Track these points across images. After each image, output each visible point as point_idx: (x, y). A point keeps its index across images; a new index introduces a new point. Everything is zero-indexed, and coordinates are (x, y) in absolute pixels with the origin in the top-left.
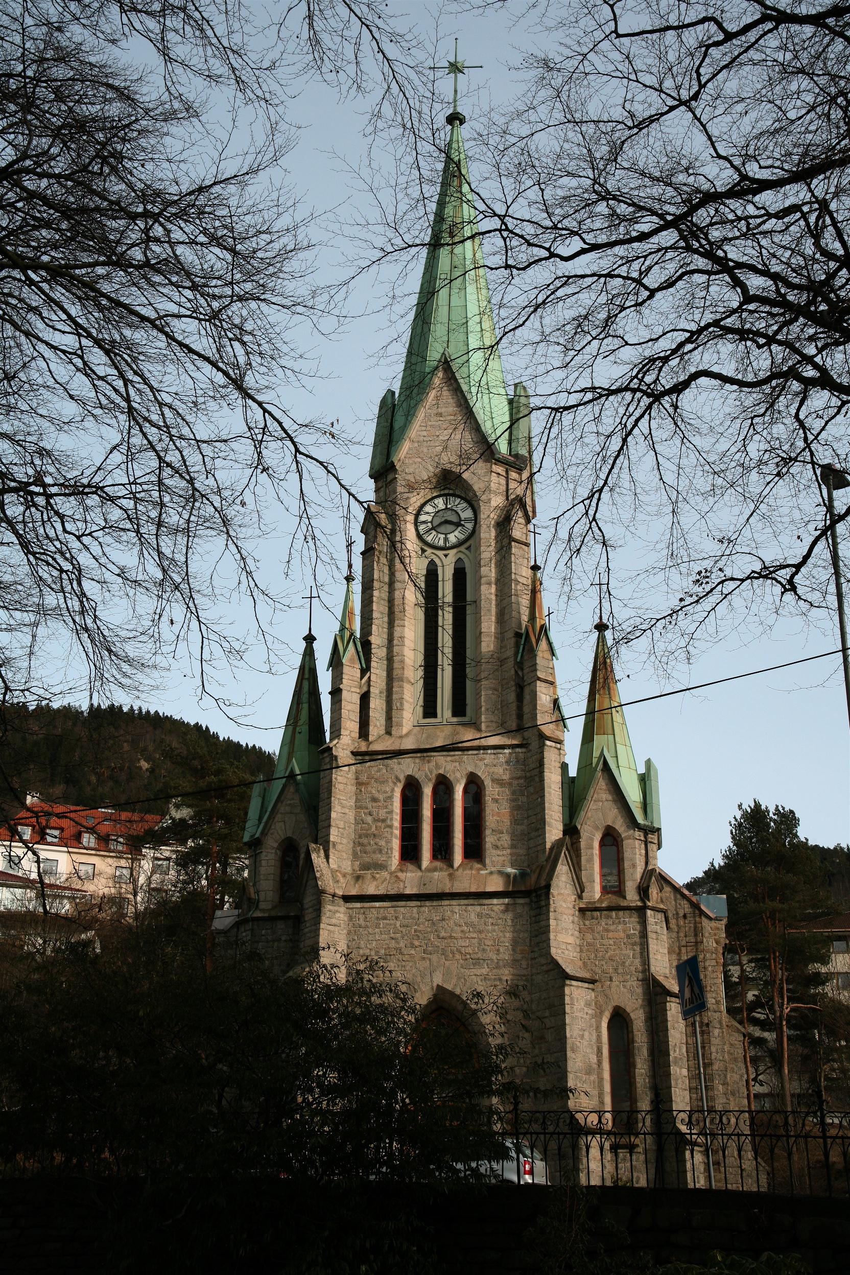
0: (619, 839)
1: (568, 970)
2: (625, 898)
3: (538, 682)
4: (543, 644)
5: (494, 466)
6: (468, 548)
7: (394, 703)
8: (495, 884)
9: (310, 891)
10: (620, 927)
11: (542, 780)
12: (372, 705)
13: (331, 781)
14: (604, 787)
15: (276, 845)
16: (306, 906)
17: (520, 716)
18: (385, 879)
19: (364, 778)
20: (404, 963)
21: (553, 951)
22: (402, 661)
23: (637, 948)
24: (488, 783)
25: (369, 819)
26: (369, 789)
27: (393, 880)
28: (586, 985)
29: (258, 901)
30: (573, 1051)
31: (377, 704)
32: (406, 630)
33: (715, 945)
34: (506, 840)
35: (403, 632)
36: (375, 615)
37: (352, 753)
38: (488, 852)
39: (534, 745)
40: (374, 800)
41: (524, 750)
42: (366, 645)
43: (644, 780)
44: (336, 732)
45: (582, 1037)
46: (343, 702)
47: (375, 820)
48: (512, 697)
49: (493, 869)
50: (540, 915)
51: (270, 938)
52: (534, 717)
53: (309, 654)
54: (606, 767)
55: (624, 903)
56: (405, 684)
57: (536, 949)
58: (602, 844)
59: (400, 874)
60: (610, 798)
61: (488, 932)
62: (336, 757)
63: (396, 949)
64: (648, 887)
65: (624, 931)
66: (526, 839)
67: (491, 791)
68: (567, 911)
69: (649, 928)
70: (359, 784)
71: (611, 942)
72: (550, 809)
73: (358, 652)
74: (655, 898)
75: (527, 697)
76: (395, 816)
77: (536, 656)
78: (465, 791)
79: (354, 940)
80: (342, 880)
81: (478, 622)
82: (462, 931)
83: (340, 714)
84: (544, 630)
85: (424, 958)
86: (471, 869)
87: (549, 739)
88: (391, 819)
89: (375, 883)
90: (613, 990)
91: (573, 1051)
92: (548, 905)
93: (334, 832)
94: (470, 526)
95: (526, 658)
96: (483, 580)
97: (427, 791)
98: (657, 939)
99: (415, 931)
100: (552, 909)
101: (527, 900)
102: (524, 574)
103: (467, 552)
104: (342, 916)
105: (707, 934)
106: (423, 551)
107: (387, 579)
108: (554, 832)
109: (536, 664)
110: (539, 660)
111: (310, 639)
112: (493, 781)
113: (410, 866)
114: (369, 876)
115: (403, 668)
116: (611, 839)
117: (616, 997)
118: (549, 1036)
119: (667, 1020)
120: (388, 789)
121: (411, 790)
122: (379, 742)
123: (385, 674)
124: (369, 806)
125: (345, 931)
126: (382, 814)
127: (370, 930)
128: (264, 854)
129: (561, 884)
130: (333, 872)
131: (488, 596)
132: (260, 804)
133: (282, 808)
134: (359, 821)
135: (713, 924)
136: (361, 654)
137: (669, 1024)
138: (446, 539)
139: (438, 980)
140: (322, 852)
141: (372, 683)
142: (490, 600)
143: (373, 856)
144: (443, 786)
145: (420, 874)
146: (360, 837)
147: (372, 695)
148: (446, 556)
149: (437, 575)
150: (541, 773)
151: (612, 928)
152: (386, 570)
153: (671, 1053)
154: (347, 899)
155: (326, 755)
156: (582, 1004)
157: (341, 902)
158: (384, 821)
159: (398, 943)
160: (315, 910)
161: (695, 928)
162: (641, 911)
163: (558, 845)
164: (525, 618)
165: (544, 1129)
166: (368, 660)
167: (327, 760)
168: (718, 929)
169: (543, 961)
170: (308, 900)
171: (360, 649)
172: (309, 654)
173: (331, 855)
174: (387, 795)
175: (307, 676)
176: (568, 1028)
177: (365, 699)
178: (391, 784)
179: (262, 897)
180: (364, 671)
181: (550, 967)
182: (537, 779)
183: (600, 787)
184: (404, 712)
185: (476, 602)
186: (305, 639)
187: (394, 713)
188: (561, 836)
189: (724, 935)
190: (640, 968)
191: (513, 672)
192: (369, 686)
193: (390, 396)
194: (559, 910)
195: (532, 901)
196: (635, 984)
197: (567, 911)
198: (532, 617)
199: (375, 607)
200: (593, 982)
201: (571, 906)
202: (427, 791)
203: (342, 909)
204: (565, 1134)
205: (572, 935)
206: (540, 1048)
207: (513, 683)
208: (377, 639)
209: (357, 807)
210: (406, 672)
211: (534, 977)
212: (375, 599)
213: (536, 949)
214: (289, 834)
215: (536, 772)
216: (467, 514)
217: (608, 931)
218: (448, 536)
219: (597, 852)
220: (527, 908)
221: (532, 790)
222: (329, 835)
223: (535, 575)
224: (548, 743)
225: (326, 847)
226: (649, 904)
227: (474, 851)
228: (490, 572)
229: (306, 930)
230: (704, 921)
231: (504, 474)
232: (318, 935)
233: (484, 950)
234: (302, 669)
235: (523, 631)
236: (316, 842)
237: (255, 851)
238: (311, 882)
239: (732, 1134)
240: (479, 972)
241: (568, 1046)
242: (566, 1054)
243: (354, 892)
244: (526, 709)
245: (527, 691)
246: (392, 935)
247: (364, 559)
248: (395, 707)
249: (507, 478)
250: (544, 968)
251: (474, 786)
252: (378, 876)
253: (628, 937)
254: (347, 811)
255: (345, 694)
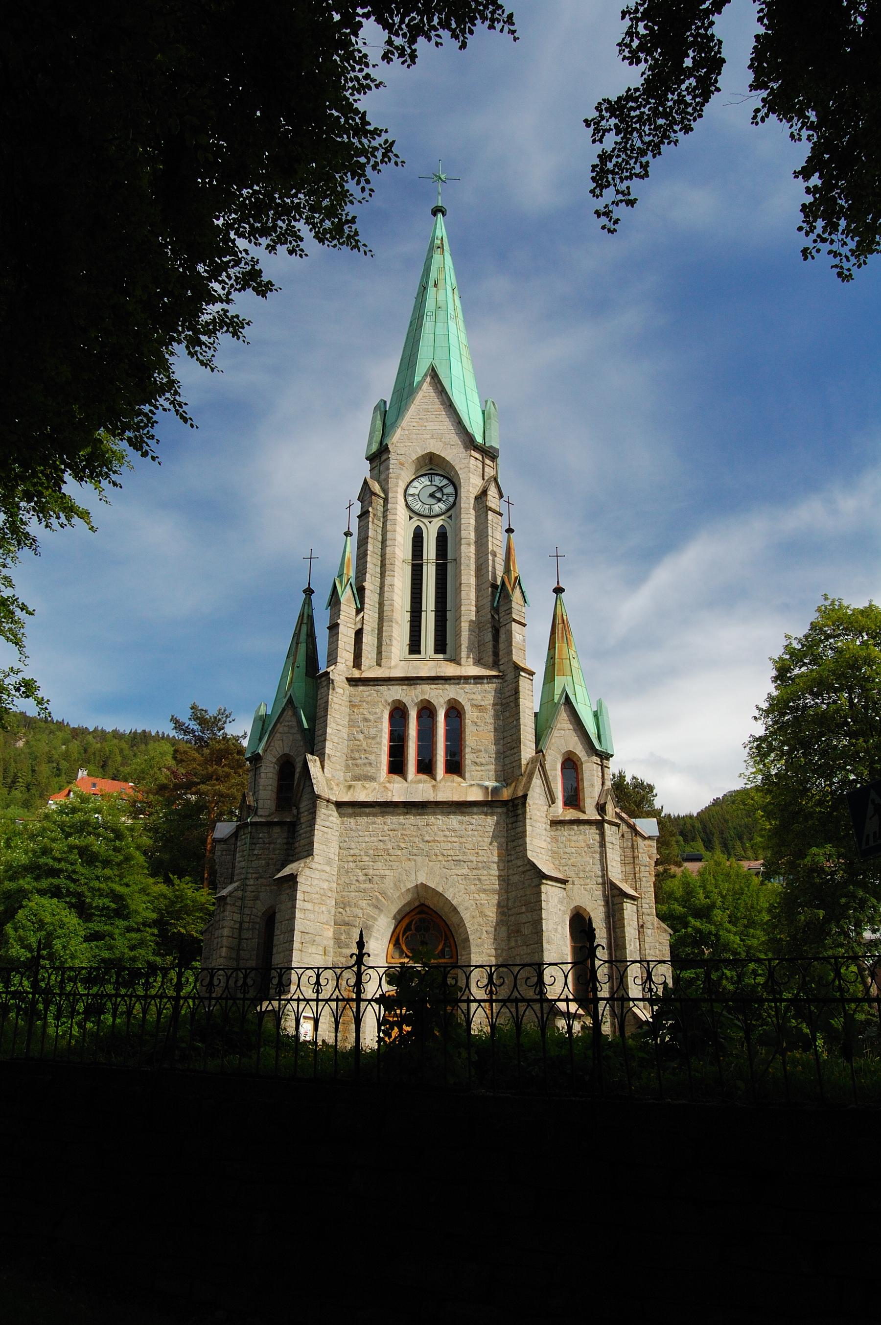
0: (579, 763)
1: (544, 871)
2: (584, 812)
3: (513, 623)
4: (517, 591)
5: (472, 452)
6: (450, 517)
7: (384, 639)
8: (476, 795)
9: (306, 796)
10: (581, 837)
11: (517, 705)
12: (364, 640)
13: (327, 702)
14: (566, 718)
15: (274, 760)
16: (302, 810)
17: (496, 654)
18: (375, 789)
19: (356, 700)
20: (391, 863)
21: (530, 855)
22: (392, 605)
23: (597, 856)
24: (468, 707)
25: (360, 736)
26: (361, 710)
27: (382, 789)
28: (559, 885)
29: (257, 809)
30: (548, 943)
31: (369, 640)
32: (396, 579)
33: (648, 859)
34: (484, 758)
35: (393, 581)
36: (369, 565)
37: (347, 679)
38: (467, 768)
39: (510, 676)
40: (366, 720)
41: (500, 681)
42: (360, 592)
43: (596, 715)
44: (332, 659)
45: (556, 930)
46: (340, 635)
47: (366, 738)
48: (489, 637)
49: (473, 783)
50: (516, 822)
51: (266, 841)
52: (510, 653)
53: (308, 602)
54: (568, 701)
55: (583, 817)
56: (394, 624)
57: (513, 852)
58: (563, 767)
59: (388, 785)
60: (571, 727)
61: (468, 836)
62: (333, 680)
63: (384, 850)
64: (605, 803)
65: (585, 842)
66: (502, 756)
67: (470, 715)
68: (540, 819)
69: (607, 839)
70: (352, 705)
71: (573, 850)
72: (524, 730)
73: (354, 594)
74: (610, 814)
75: (503, 637)
76: (384, 735)
77: (511, 601)
78: (447, 716)
79: (345, 841)
80: (335, 788)
81: (458, 575)
82: (445, 836)
83: (338, 645)
84: (518, 581)
85: (409, 859)
86: (453, 781)
87: (524, 670)
88: (381, 737)
89: (365, 792)
90: (575, 891)
91: (548, 943)
92: (525, 812)
93: (328, 744)
94: (451, 499)
95: (501, 603)
96: (463, 541)
97: (413, 714)
98: (613, 849)
99: (402, 835)
100: (528, 817)
101: (504, 810)
102: (498, 538)
103: (448, 520)
104: (334, 819)
105: (641, 851)
106: (411, 518)
107: (380, 538)
108: (528, 751)
109: (511, 608)
110: (514, 605)
111: (309, 592)
112: (472, 705)
113: (396, 778)
114: (360, 786)
115: (393, 611)
116: (571, 764)
117: (577, 898)
118: (526, 930)
119: (623, 919)
120: (378, 710)
121: (398, 713)
122: (370, 671)
123: (377, 615)
124: (361, 724)
125: (337, 833)
126: (373, 731)
127: (360, 833)
128: (263, 767)
129: (536, 795)
130: (328, 781)
131: (467, 554)
132: (260, 727)
133: (280, 728)
134: (352, 738)
135: (647, 842)
136: (356, 596)
137: (626, 922)
138: (430, 509)
139: (422, 879)
140: (318, 763)
141: (365, 622)
142: (469, 557)
143: (363, 768)
144: (427, 711)
145: (406, 785)
146: (352, 751)
147: (364, 631)
148: (430, 522)
149: (422, 538)
150: (517, 699)
151: (574, 838)
152: (380, 530)
153: (628, 946)
154: (339, 805)
155: (324, 679)
156: (556, 901)
157: (333, 807)
158: (373, 738)
159: (386, 845)
160: (310, 813)
161: (633, 845)
162: (599, 825)
163: (533, 761)
164: (500, 573)
165: (211, 992)
166: (362, 603)
167: (325, 683)
168: (651, 846)
169: (519, 863)
170: (304, 805)
171: (355, 592)
172: (308, 602)
173: (326, 766)
174: (377, 716)
175: (305, 621)
176: (544, 921)
177: (359, 634)
178: (381, 707)
179: (260, 806)
180: (359, 611)
181: (528, 867)
182: (512, 705)
183: (563, 720)
184: (393, 648)
185: (457, 561)
186: (304, 592)
187: (384, 648)
188: (534, 754)
189: (656, 852)
190: (600, 873)
191: (489, 616)
192: (363, 624)
193: (382, 403)
194: (534, 818)
195: (508, 810)
196: (594, 887)
197: (540, 819)
198: (507, 570)
199: (369, 559)
200: (564, 882)
201: (544, 816)
202: (413, 714)
203: (335, 814)
204: (308, 1001)
205: (545, 841)
206: (516, 941)
207: (489, 625)
208: (371, 585)
209: (350, 726)
210: (394, 614)
211: (510, 877)
212: (369, 552)
213: (513, 852)
214: (287, 751)
215: (512, 698)
216: (450, 490)
217: (569, 840)
218: (432, 506)
219: (560, 774)
220: (504, 817)
221: (507, 714)
222: (324, 748)
223: (509, 537)
224: (522, 674)
225: (322, 756)
226: (606, 818)
227: (455, 767)
228: (469, 532)
229: (302, 831)
230: (639, 840)
231: (481, 459)
232: (313, 835)
233: (464, 852)
234: (302, 616)
235: (499, 583)
236: (312, 754)
237: (255, 765)
238: (307, 789)
239: (330, 1000)
240: (459, 872)
241: (544, 939)
242: (542, 946)
243: (346, 798)
244: (502, 646)
245: (502, 631)
246: (381, 838)
247: (360, 522)
248: (384, 643)
249: (483, 463)
250: (521, 869)
251: (455, 712)
252: (367, 786)
253: (589, 846)
254: (340, 728)
255: (342, 629)
